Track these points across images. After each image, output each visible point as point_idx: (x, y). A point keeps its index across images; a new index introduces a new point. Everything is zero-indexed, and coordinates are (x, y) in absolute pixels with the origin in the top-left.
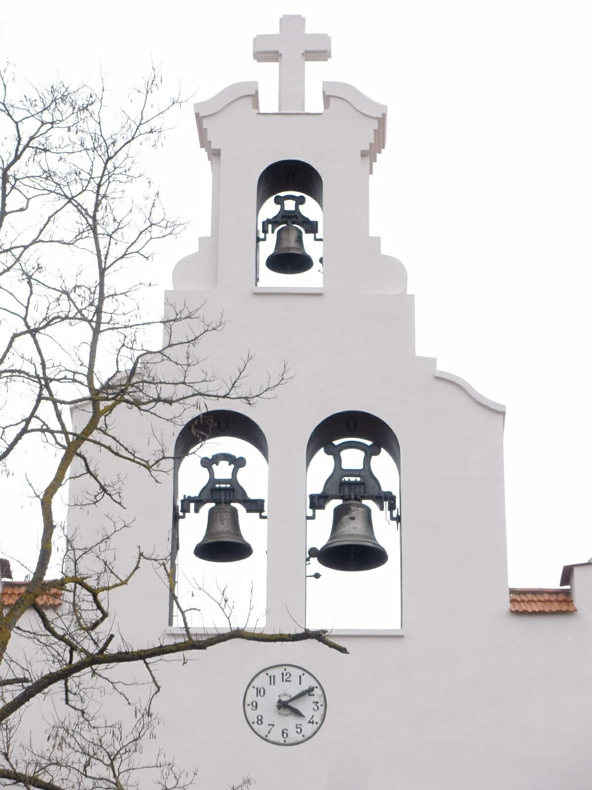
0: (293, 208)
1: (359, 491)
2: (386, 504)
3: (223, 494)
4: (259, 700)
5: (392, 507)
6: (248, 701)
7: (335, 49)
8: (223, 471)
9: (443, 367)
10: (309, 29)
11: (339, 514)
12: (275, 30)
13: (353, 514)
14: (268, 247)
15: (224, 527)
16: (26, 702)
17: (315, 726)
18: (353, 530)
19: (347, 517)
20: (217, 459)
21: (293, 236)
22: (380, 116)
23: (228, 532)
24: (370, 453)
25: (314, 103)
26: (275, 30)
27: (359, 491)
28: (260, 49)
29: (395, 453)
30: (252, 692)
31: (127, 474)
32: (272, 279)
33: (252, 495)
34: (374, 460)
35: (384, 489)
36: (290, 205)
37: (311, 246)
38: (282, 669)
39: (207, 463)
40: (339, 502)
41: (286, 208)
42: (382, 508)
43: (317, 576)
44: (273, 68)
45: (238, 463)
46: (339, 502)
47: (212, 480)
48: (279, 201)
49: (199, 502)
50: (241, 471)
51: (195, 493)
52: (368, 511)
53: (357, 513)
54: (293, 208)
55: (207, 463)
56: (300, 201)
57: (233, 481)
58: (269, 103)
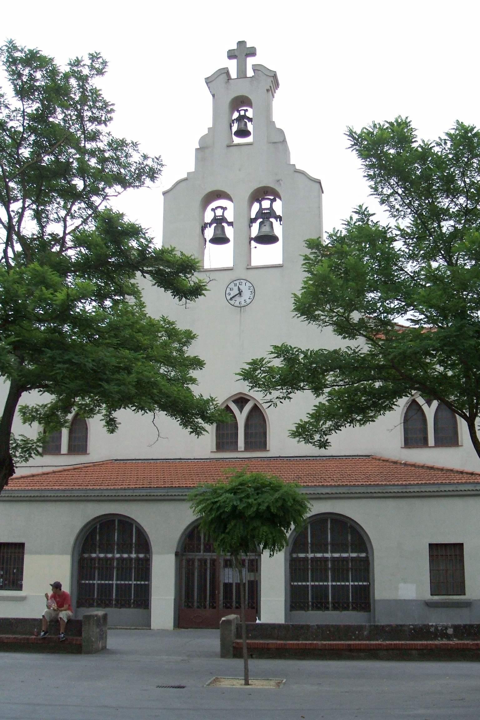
0: (244, 114)
1: (268, 216)
2: (278, 220)
3: (219, 220)
4: (231, 292)
5: (280, 221)
6: (227, 293)
7: (258, 52)
8: (219, 212)
9: (298, 167)
10: (248, 45)
11: (261, 224)
12: (235, 47)
13: (265, 224)
14: (235, 128)
15: (219, 232)
16: (475, 419)
17: (251, 300)
18: (266, 229)
19: (263, 225)
20: (217, 208)
21: (243, 123)
22: (273, 75)
23: (221, 234)
24: (273, 201)
25: (250, 73)
26: (235, 47)
27: (268, 216)
28: (230, 55)
29: (280, 198)
30: (228, 289)
31: (300, 255)
32: (237, 140)
33: (229, 220)
34: (274, 204)
35: (278, 214)
36: (242, 113)
37: (250, 127)
38: (239, 281)
39: (213, 210)
40: (262, 220)
41: (241, 114)
42: (277, 221)
43: (256, 247)
44: (234, 62)
45: (224, 209)
46: (262, 220)
47: (215, 216)
48: (239, 111)
49: (210, 224)
50: (226, 212)
51: (209, 221)
52: (272, 223)
53: (267, 224)
54: (244, 114)
55: (213, 210)
56: (246, 111)
57: (223, 216)
58: (234, 75)
